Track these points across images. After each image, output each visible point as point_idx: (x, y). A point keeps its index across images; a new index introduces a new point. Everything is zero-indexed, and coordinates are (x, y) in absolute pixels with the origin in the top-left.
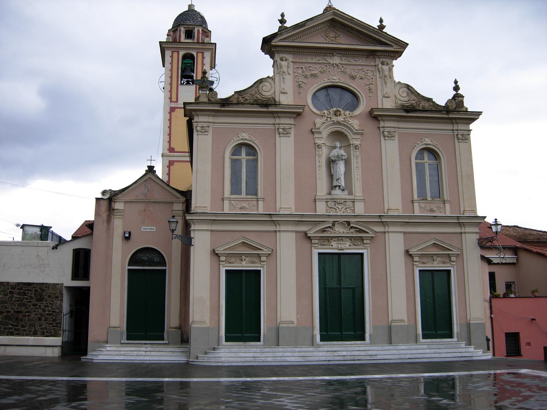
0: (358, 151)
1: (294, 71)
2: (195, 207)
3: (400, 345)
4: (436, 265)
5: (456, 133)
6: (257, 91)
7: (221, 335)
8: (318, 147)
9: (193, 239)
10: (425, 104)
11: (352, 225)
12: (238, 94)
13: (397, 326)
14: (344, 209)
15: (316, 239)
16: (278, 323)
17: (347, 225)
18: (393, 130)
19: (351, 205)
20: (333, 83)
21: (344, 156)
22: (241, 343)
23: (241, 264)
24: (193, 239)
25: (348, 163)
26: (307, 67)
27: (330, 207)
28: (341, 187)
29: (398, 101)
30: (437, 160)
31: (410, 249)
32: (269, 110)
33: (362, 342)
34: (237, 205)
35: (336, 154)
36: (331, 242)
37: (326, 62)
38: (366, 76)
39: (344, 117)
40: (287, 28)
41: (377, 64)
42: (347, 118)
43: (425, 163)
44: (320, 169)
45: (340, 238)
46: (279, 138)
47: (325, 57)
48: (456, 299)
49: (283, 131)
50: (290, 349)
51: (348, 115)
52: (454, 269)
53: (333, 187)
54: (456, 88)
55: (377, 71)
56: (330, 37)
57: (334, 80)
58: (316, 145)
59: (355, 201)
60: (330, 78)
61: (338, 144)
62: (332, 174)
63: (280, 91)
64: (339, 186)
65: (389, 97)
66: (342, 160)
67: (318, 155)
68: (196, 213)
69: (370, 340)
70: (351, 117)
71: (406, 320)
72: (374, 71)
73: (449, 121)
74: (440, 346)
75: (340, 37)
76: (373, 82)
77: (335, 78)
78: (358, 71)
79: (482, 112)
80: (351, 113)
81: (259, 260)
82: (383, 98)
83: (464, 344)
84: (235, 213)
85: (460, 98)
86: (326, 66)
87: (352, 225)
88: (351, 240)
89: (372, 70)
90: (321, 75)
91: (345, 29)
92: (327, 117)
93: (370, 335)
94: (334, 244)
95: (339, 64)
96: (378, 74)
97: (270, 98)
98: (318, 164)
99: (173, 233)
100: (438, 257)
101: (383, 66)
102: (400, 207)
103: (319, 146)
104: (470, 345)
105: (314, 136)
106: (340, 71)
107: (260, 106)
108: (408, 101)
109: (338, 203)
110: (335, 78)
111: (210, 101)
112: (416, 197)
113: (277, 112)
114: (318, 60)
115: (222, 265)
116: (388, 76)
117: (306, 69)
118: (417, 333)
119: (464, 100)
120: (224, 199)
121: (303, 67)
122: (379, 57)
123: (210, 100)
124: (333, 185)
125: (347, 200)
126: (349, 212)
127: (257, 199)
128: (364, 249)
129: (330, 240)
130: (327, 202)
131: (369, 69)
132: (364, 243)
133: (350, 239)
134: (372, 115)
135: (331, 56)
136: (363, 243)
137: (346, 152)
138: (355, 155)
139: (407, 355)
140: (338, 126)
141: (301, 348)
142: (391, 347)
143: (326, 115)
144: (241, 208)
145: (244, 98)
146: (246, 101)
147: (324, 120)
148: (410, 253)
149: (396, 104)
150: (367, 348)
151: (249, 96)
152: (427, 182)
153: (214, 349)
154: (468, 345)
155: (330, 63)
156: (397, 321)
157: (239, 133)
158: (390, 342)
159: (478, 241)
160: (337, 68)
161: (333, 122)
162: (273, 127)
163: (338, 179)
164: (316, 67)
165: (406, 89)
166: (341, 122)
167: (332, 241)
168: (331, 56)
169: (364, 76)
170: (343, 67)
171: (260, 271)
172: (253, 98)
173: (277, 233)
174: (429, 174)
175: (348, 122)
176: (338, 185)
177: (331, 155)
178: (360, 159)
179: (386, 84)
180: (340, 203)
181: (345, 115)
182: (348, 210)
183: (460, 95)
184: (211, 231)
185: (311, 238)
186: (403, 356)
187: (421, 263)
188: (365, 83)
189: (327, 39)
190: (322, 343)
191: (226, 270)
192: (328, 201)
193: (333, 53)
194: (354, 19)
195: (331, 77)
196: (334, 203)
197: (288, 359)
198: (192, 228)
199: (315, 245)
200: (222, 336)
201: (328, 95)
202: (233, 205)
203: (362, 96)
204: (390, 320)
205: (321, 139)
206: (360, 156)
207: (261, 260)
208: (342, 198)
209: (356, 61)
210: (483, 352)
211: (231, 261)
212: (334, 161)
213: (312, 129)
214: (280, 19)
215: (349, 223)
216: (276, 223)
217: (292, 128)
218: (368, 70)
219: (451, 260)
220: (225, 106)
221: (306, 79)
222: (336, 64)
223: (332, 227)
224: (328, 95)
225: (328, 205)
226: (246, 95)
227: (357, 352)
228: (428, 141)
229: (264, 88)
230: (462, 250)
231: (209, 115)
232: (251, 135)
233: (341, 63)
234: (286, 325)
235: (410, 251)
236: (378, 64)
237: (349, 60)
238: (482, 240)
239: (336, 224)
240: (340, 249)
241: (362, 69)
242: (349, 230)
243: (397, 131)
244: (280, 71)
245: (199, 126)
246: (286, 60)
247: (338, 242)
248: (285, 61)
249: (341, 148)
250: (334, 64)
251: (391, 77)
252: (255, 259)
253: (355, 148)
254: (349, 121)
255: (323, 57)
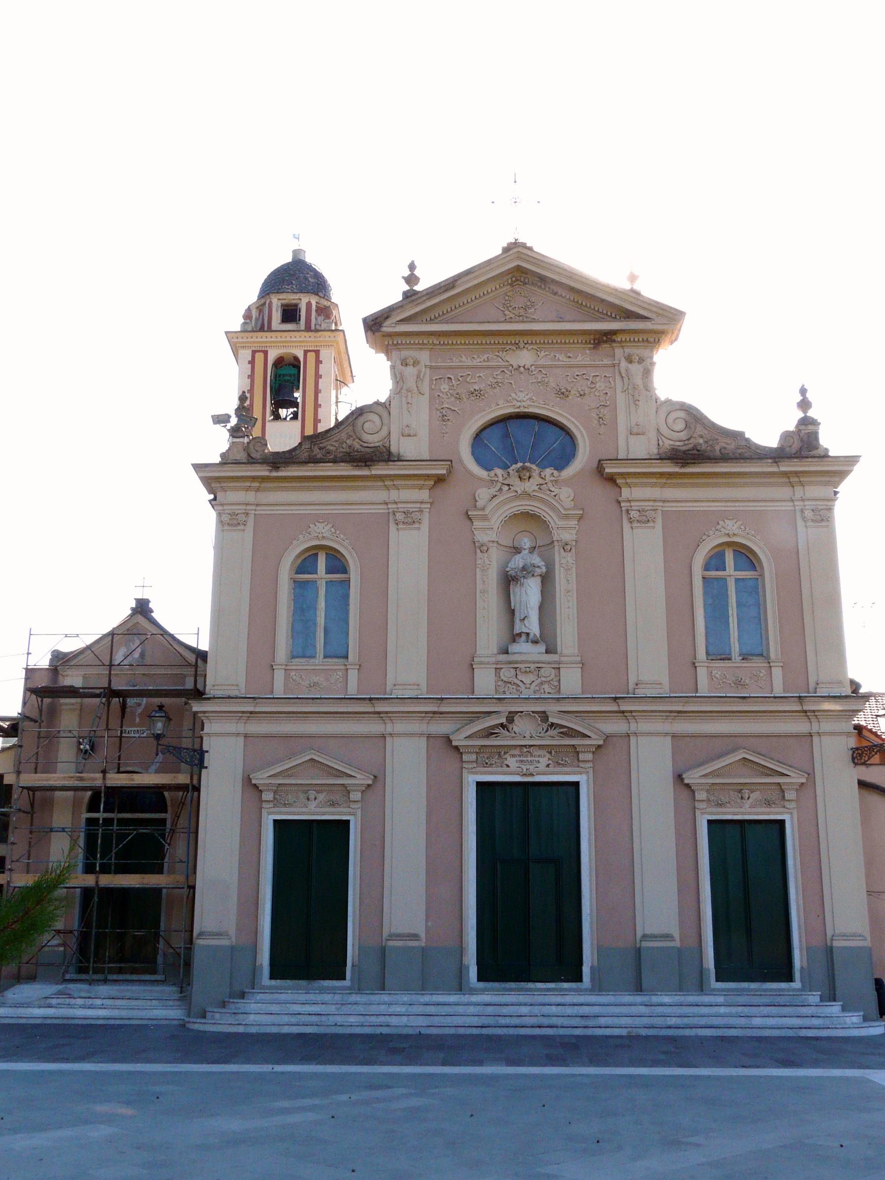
0: (571, 556)
3: (513, 993)
4: (749, 810)
6: (352, 434)
8: (481, 549)
9: (206, 754)
11: (551, 720)
15: (471, 753)
16: (828, 939)
18: (239, 509)
19: (553, 676)
20: (518, 408)
21: (539, 567)
24: (206, 754)
27: (505, 681)
28: (531, 636)
31: (687, 770)
32: (374, 472)
33: (573, 985)
34: (302, 679)
35: (521, 565)
36: (506, 759)
37: (504, 364)
39: (542, 481)
40: (418, 292)
41: (618, 362)
42: (546, 483)
43: (728, 579)
45: (525, 750)
47: (501, 353)
48: (797, 888)
49: (814, 515)
50: (405, 998)
52: (792, 818)
53: (515, 638)
54: (804, 405)
55: (618, 377)
57: (520, 401)
58: (477, 545)
60: (510, 398)
63: (401, 427)
64: (528, 634)
68: (214, 698)
70: (556, 481)
72: (609, 377)
75: (536, 307)
77: (521, 396)
79: (860, 456)
80: (556, 473)
82: (402, 437)
84: (296, 696)
86: (503, 371)
87: (551, 720)
88: (550, 753)
89: (605, 376)
91: (547, 289)
93: (591, 967)
94: (512, 762)
97: (379, 447)
99: (160, 742)
100: (318, 792)
101: (630, 366)
102: (665, 680)
103: (482, 548)
104: (835, 1000)
106: (534, 381)
107: (353, 466)
108: (688, 440)
110: (521, 396)
111: (252, 458)
114: (486, 359)
115: (267, 810)
118: (704, 966)
119: (820, 432)
120: (697, 665)
121: (452, 377)
123: (252, 455)
124: (515, 633)
125: (543, 665)
126: (547, 690)
127: (346, 665)
128: (580, 773)
129: (503, 753)
131: (597, 374)
132: (580, 759)
133: (548, 752)
134: (603, 475)
135: (513, 350)
136: (578, 759)
139: (668, 1018)
142: (639, 999)
143: (501, 479)
144: (311, 687)
146: (328, 455)
147: (495, 490)
149: (659, 449)
152: (731, 619)
153: (242, 995)
154: (830, 1001)
156: (654, 937)
157: (311, 525)
158: (639, 988)
159: (851, 752)
161: (516, 494)
163: (524, 619)
164: (481, 375)
166: (532, 494)
167: (507, 756)
168: (515, 348)
169: (587, 391)
172: (343, 448)
173: (387, 739)
174: (737, 602)
178: (574, 575)
179: (636, 405)
180: (526, 672)
181: (542, 478)
182: (546, 686)
185: (461, 751)
187: (713, 804)
189: (507, 312)
191: (275, 821)
193: (517, 344)
195: (513, 395)
197: (394, 1021)
198: (206, 730)
202: (293, 680)
203: (582, 435)
204: (385, 935)
207: (349, 798)
209: (570, 357)
210: (865, 1019)
213: (467, 510)
215: (544, 716)
216: (818, 717)
217: (425, 510)
218: (597, 376)
219: (784, 797)
220: (279, 468)
222: (524, 367)
224: (507, 435)
225: (500, 677)
226: (327, 443)
229: (366, 426)
231: (654, 485)
237: (555, 356)
238: (860, 752)
239: (515, 718)
240: (525, 774)
241: (584, 374)
242: (545, 730)
243: (660, 508)
245: (633, 508)
246: (416, 363)
247: (522, 758)
248: (637, 364)
249: (532, 549)
250: (520, 367)
253: (563, 548)
255: (497, 354)
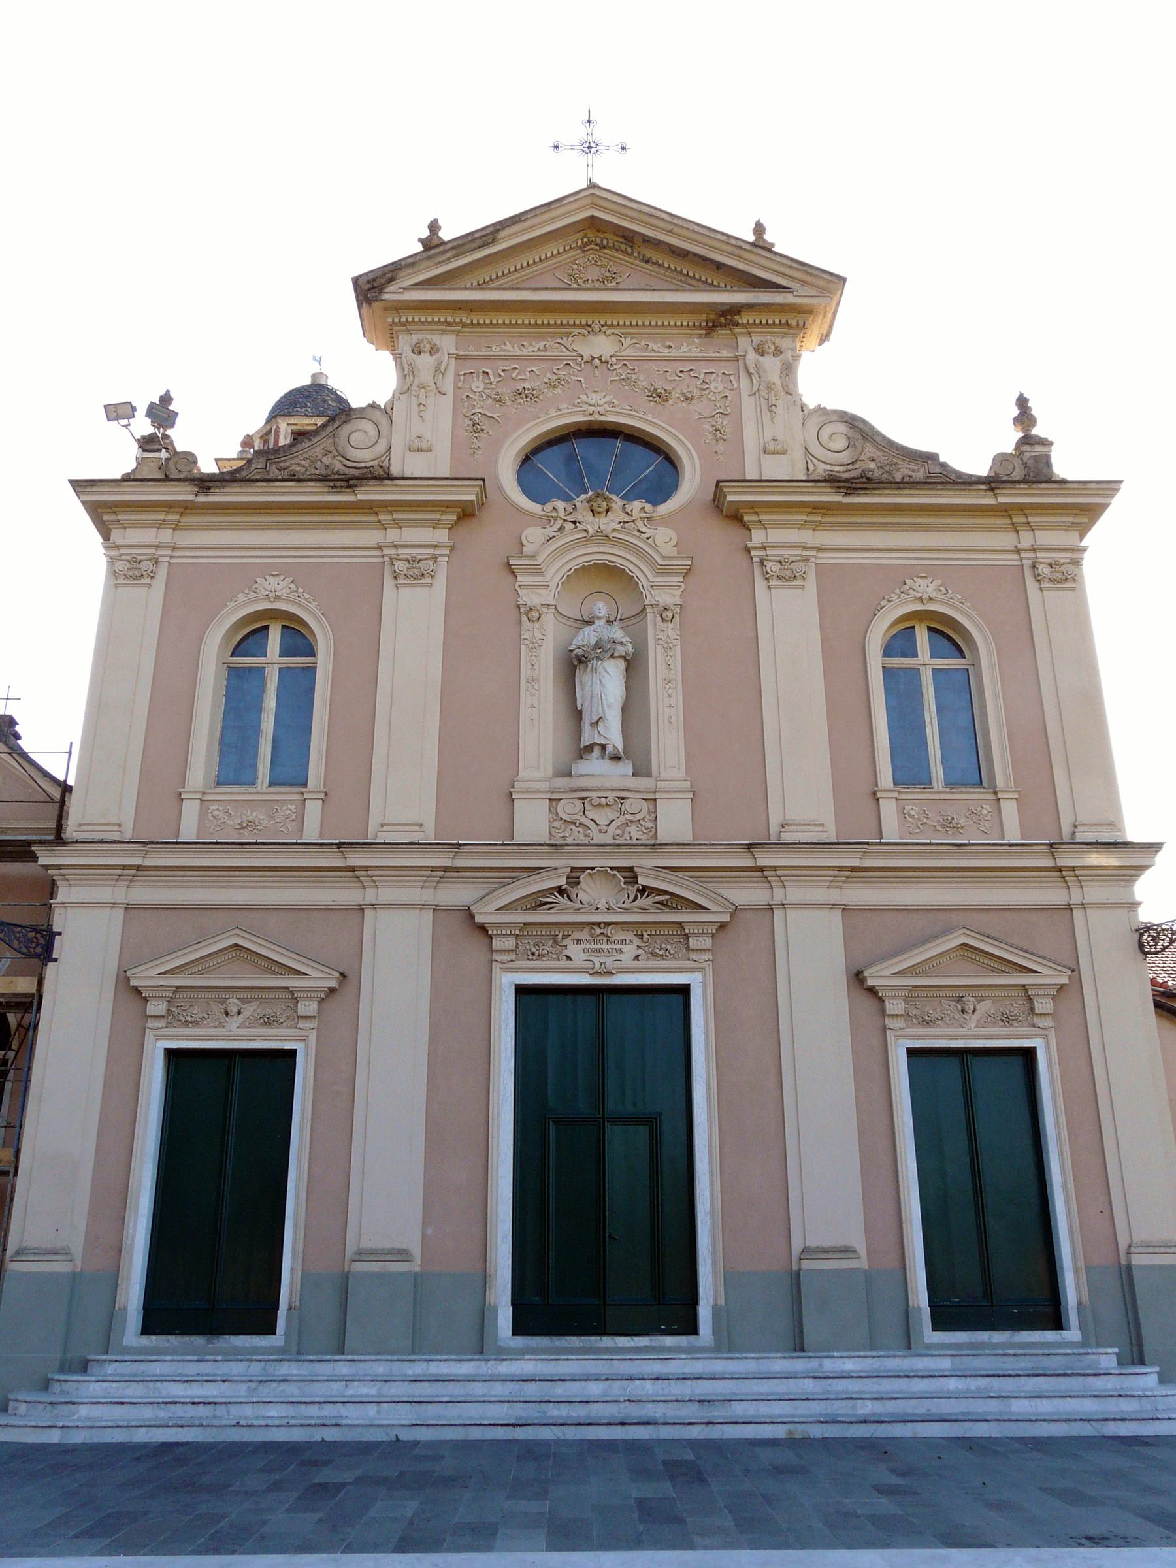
1: (460, 385)
2: (80, 825)
5: (1030, 562)
6: (331, 449)
7: (122, 1306)
9: (57, 937)
10: (913, 471)
11: (642, 881)
12: (265, 458)
13: (822, 1272)
14: (617, 828)
17: (625, 883)
19: (645, 812)
21: (621, 643)
22: (198, 1341)
23: (224, 1027)
24: (57, 937)
25: (634, 665)
26: (503, 371)
28: (610, 749)
29: (814, 465)
30: (962, 655)
31: (869, 966)
32: (360, 497)
34: (230, 816)
35: (593, 641)
38: (704, 392)
41: (743, 354)
43: (922, 669)
44: (533, 691)
45: (599, 931)
46: (395, 591)
47: (565, 339)
51: (636, 514)
55: (742, 374)
56: (584, 282)
59: (658, 795)
61: (602, 608)
62: (579, 708)
64: (603, 747)
65: (784, 452)
66: (612, 656)
67: (526, 642)
69: (716, 1331)
71: (862, 1250)
72: (730, 375)
73: (999, 521)
74: (1009, 1365)
76: (728, 408)
77: (594, 398)
78: (677, 378)
79: (1121, 482)
80: (648, 507)
81: (290, 1012)
83: (1114, 1358)
85: (1038, 448)
87: (642, 881)
88: (641, 937)
90: (550, 395)
91: (636, 254)
92: (565, 520)
94: (576, 951)
95: (611, 356)
96: (744, 381)
98: (525, 671)
101: (761, 358)
103: (532, 614)
104: (1142, 1363)
105: (518, 583)
109: (596, 802)
110: (594, 398)
112: (886, 778)
113: (388, 506)
114: (542, 348)
116: (780, 388)
117: (500, 376)
122: (749, 333)
128: (691, 970)
130: (554, 804)
137: (627, 634)
138: (661, 642)
140: (602, 550)
141: (424, 1364)
142: (799, 1365)
143: (562, 514)
145: (284, 469)
148: (870, 982)
150: (698, 1367)
151: (303, 462)
152: (928, 730)
155: (582, 356)
158: (799, 1346)
160: (607, 371)
161: (585, 535)
162: (376, 557)
164: (534, 369)
165: (842, 428)
167: (568, 941)
169: (696, 393)
170: (624, 367)
171: (293, 1053)
175: (638, 534)
176: (596, 744)
177: (574, 642)
180: (600, 805)
181: (628, 514)
183: (1037, 440)
184: (126, 908)
185: (490, 932)
186: (840, 1408)
188: (700, 414)
190: (520, 1341)
192: (561, 799)
193: (590, 326)
194: (658, 214)
195: (584, 397)
196: (579, 803)
199: (505, 958)
200: (125, 1309)
201: (571, 458)
202: (214, 817)
204: (796, 1248)
205: (540, 591)
206: (679, 643)
208: (608, 785)
211: (189, 1018)
212: (582, 660)
214: (424, 237)
218: (712, 373)
219: (1032, 1009)
221: (498, 406)
222: (600, 359)
223: (565, 889)
224: (571, 458)
226: (293, 462)
227: (649, 1384)
228: (925, 587)
230: (1075, 970)
232: (297, 587)
233: (618, 354)
234: (375, 1267)
235: (866, 974)
236: (746, 352)
241: (691, 370)
244: (411, 385)
246: (433, 350)
250: (593, 358)
251: (790, 390)
252: (277, 1010)
254: (642, 532)
